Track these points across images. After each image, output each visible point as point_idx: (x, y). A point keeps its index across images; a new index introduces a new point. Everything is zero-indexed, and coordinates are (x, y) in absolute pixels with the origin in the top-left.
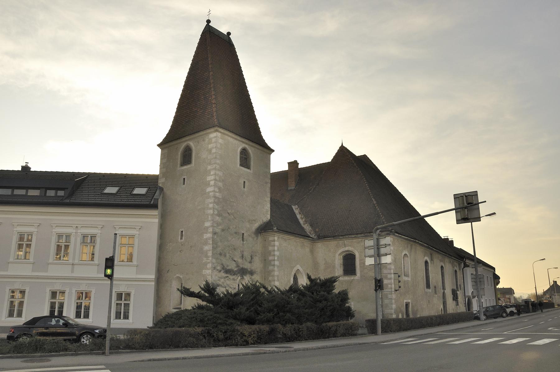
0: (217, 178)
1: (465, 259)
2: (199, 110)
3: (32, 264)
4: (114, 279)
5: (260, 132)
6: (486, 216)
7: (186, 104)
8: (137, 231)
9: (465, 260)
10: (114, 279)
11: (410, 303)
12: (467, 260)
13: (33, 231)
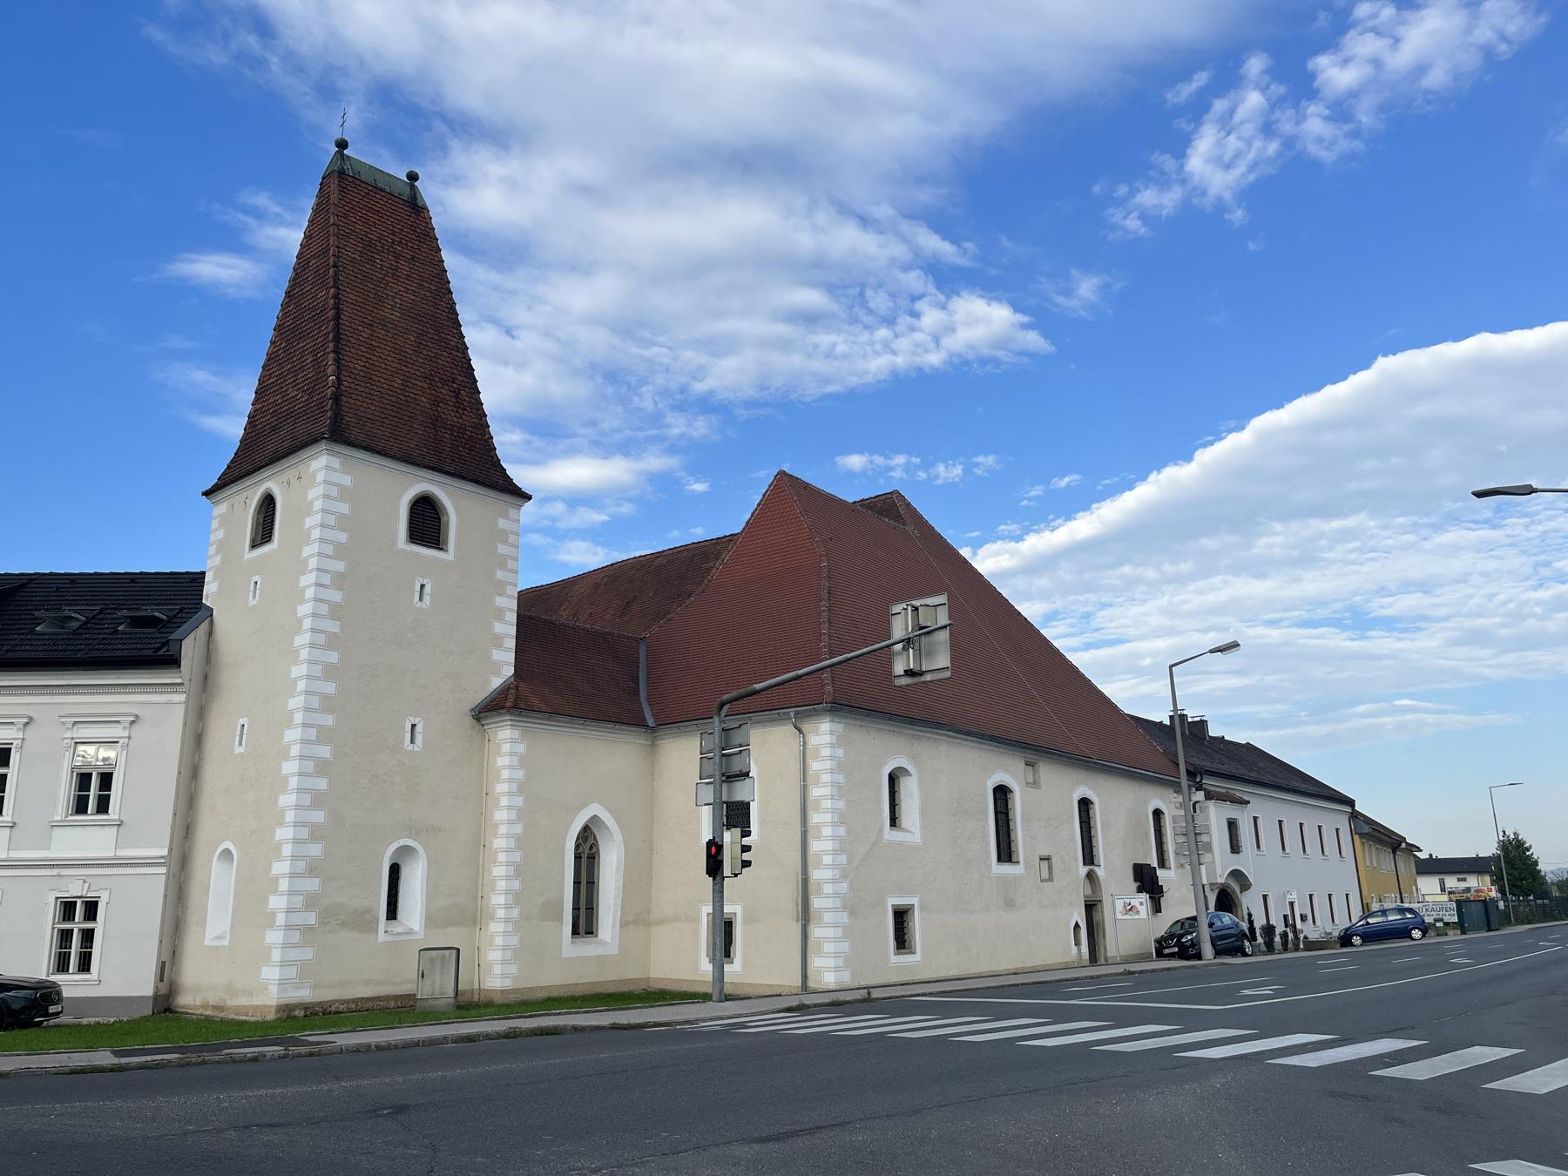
0: (326, 580)
1: (1201, 776)
2: (300, 396)
3: (8, 830)
4: (163, 870)
5: (1522, 328)
6: (1212, 651)
7: (275, 378)
8: (124, 728)
9: (1202, 779)
10: (163, 870)
11: (916, 907)
12: (1204, 776)
13: (13, 739)
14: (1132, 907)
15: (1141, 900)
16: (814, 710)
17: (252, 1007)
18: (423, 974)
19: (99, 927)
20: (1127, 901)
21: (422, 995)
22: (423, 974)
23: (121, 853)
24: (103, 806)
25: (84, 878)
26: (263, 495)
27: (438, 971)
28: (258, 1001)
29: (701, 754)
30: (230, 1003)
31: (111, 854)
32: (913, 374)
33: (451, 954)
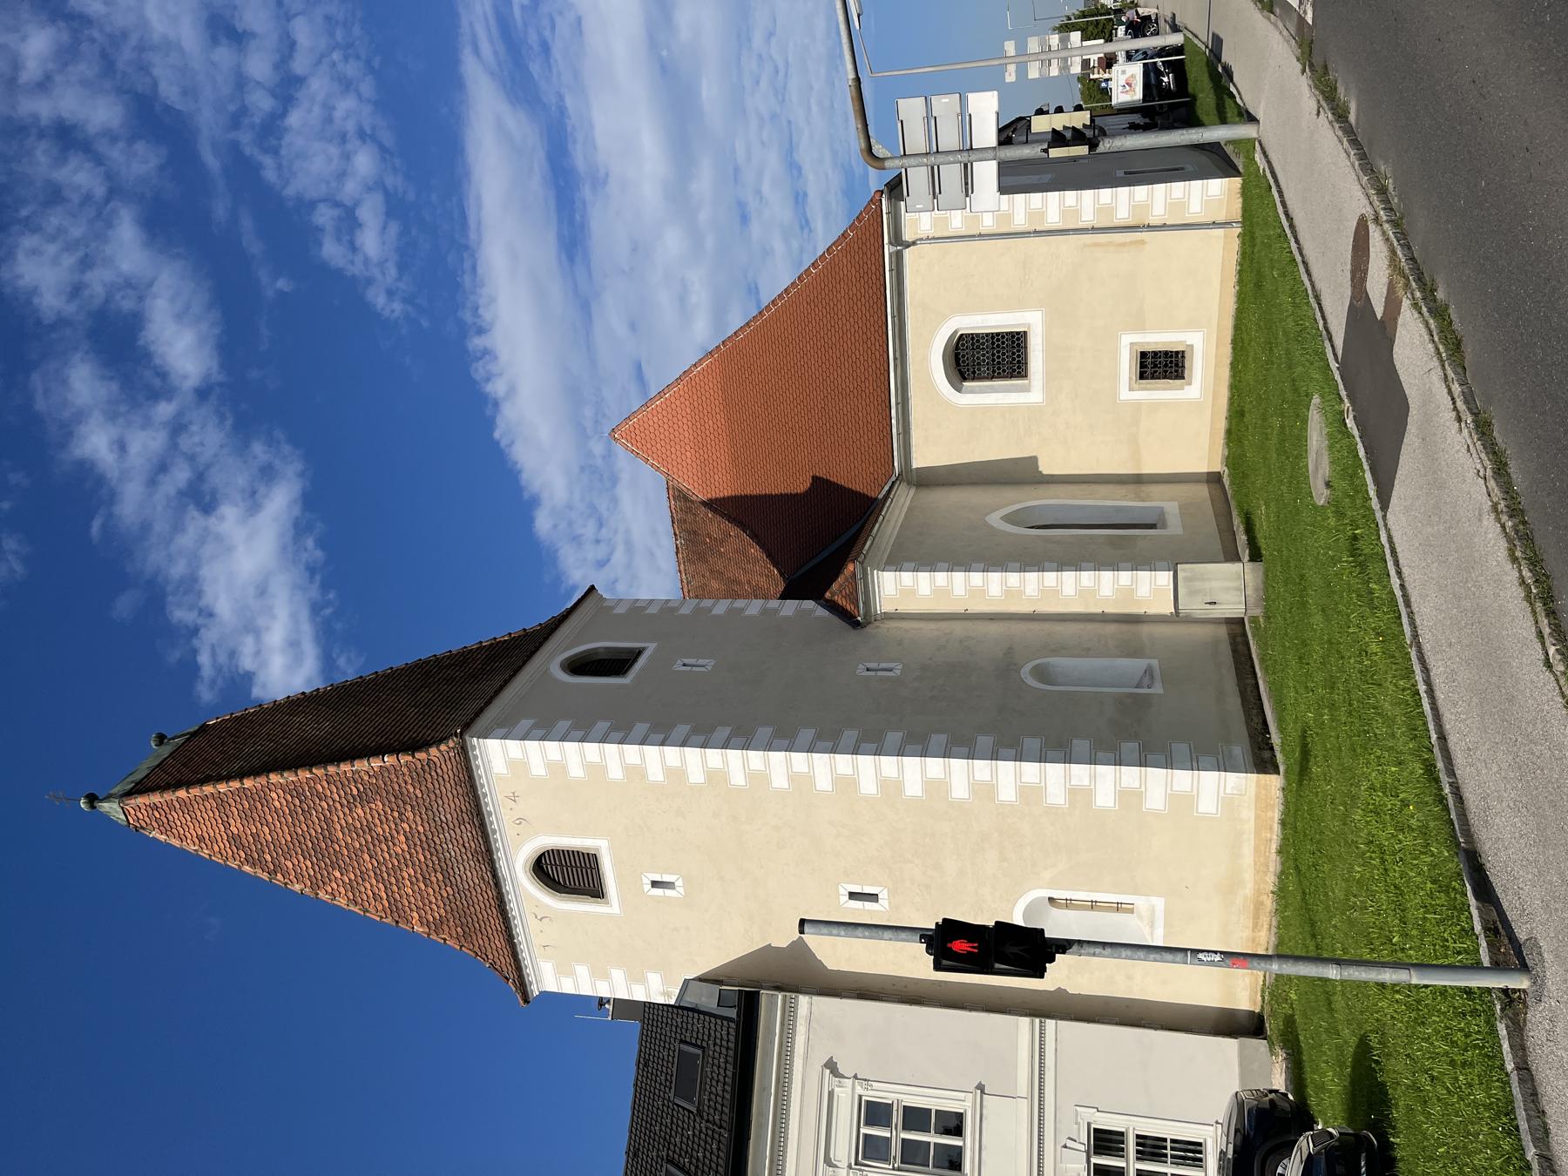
14: (1127, 84)
15: (1120, 72)
16: (891, 513)
17: (1257, 832)
18: (1210, 603)
19: (1133, 1126)
20: (1120, 88)
21: (1240, 603)
22: (1210, 603)
23: (1023, 1089)
24: (953, 1124)
25: (1059, 1148)
26: (530, 874)
27: (1207, 585)
28: (1248, 814)
29: (933, 210)
30: (1248, 890)
31: (1024, 1104)
32: (526, 496)
33: (1183, 570)
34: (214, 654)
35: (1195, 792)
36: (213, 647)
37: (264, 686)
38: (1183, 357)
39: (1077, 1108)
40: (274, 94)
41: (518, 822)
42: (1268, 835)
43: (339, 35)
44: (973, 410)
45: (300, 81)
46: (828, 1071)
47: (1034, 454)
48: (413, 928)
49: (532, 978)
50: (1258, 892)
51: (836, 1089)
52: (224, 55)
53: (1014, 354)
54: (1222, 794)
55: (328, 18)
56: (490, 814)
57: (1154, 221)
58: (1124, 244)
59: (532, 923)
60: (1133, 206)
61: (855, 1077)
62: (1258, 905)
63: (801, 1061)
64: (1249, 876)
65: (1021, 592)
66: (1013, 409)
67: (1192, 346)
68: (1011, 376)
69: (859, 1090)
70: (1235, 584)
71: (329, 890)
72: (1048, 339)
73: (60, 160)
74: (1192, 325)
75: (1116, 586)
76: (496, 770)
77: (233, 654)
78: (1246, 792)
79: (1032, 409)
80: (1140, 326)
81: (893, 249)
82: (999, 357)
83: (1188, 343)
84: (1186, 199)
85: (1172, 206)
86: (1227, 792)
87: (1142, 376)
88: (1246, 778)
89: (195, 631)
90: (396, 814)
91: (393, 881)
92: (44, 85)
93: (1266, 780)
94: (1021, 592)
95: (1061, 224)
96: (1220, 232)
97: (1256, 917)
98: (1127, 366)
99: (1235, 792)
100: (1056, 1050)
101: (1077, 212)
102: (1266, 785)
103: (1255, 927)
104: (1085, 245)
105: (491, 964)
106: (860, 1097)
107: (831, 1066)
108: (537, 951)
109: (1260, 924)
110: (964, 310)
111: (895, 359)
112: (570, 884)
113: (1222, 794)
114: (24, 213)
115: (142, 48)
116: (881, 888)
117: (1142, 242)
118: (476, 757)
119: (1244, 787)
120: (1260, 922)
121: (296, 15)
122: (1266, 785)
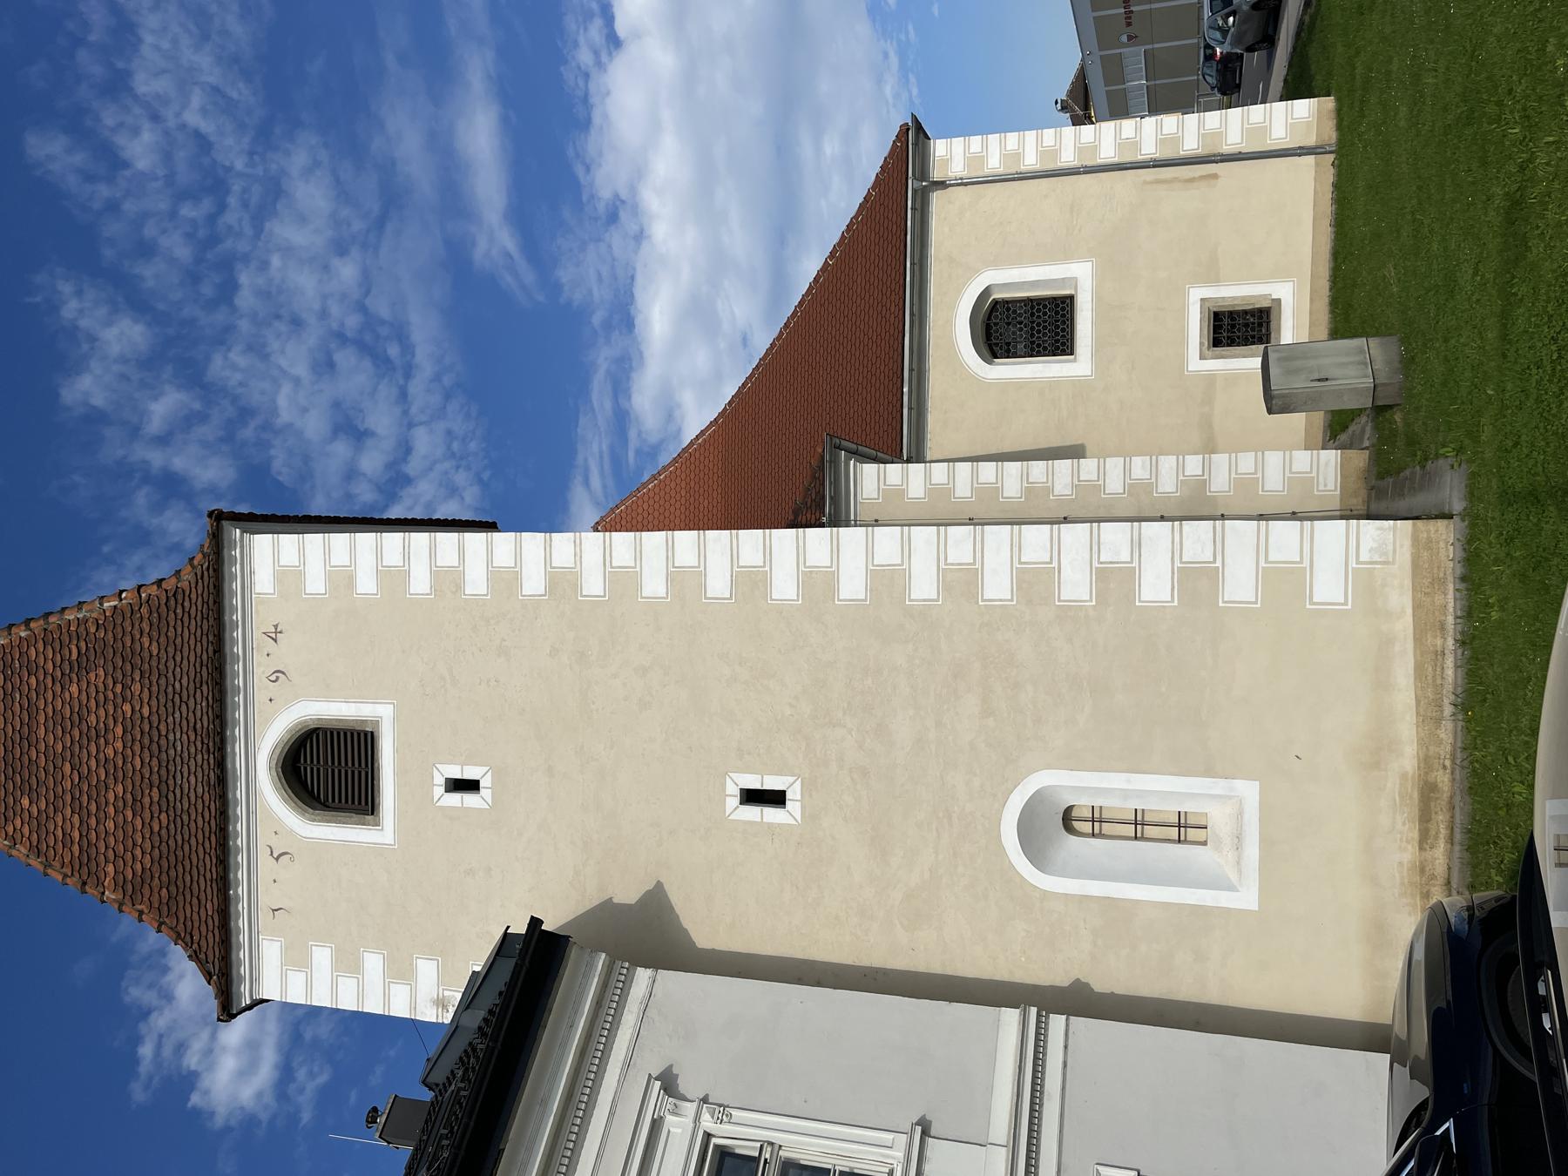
17: (1419, 639)
18: (1319, 380)
22: (1319, 380)
28: (1400, 599)
30: (1407, 759)
31: (1001, 1157)
34: (159, 1046)
35: (1306, 563)
36: (161, 1036)
37: (207, 1092)
38: (1268, 317)
39: (1100, 1168)
40: (379, 488)
41: (273, 678)
42: (1439, 642)
43: (456, 446)
44: (1005, 386)
45: (407, 481)
46: (658, 1084)
47: (1080, 442)
48: (103, 893)
49: (244, 970)
50: (1426, 763)
51: (670, 1118)
52: (341, 449)
53: (1057, 327)
54: (1353, 564)
55: (449, 433)
56: (236, 658)
57: (1226, 149)
58: (1192, 180)
59: (264, 862)
60: (1203, 134)
61: (705, 1100)
62: (1428, 791)
63: (618, 1071)
64: (1407, 730)
65: (1048, 490)
66: (1054, 384)
67: (1280, 300)
68: (1054, 352)
69: (707, 1123)
70: (1357, 358)
71: (10, 829)
72: (1098, 298)
73: (158, 507)
74: (1278, 274)
75: (1181, 478)
76: (258, 588)
77: (181, 1048)
78: (1394, 559)
79: (1077, 384)
80: (1214, 279)
81: (917, 184)
82: (1039, 331)
83: (1273, 297)
84: (1267, 123)
85: (1250, 131)
86: (1362, 559)
87: (1216, 343)
88: (1395, 529)
89: (145, 1014)
90: (119, 688)
91: (93, 807)
92: (163, 440)
93: (1428, 532)
94: (1048, 490)
95: (1116, 159)
96: (1310, 159)
97: (1425, 817)
98: (1195, 328)
99: (1376, 558)
100: (1066, 1047)
101: (1135, 144)
102: (1429, 540)
103: (1424, 840)
104: (1145, 183)
105: (195, 952)
106: (708, 1136)
107: (669, 1084)
108: (264, 918)
109: (1433, 833)
110: (997, 263)
111: (911, 370)
112: (333, 800)
113: (1353, 564)
114: (106, 549)
115: (267, 426)
116: (791, 779)
117: (1215, 176)
118: (233, 561)
119: (1391, 548)
120: (1432, 826)
121: (416, 425)
122: (1429, 540)
